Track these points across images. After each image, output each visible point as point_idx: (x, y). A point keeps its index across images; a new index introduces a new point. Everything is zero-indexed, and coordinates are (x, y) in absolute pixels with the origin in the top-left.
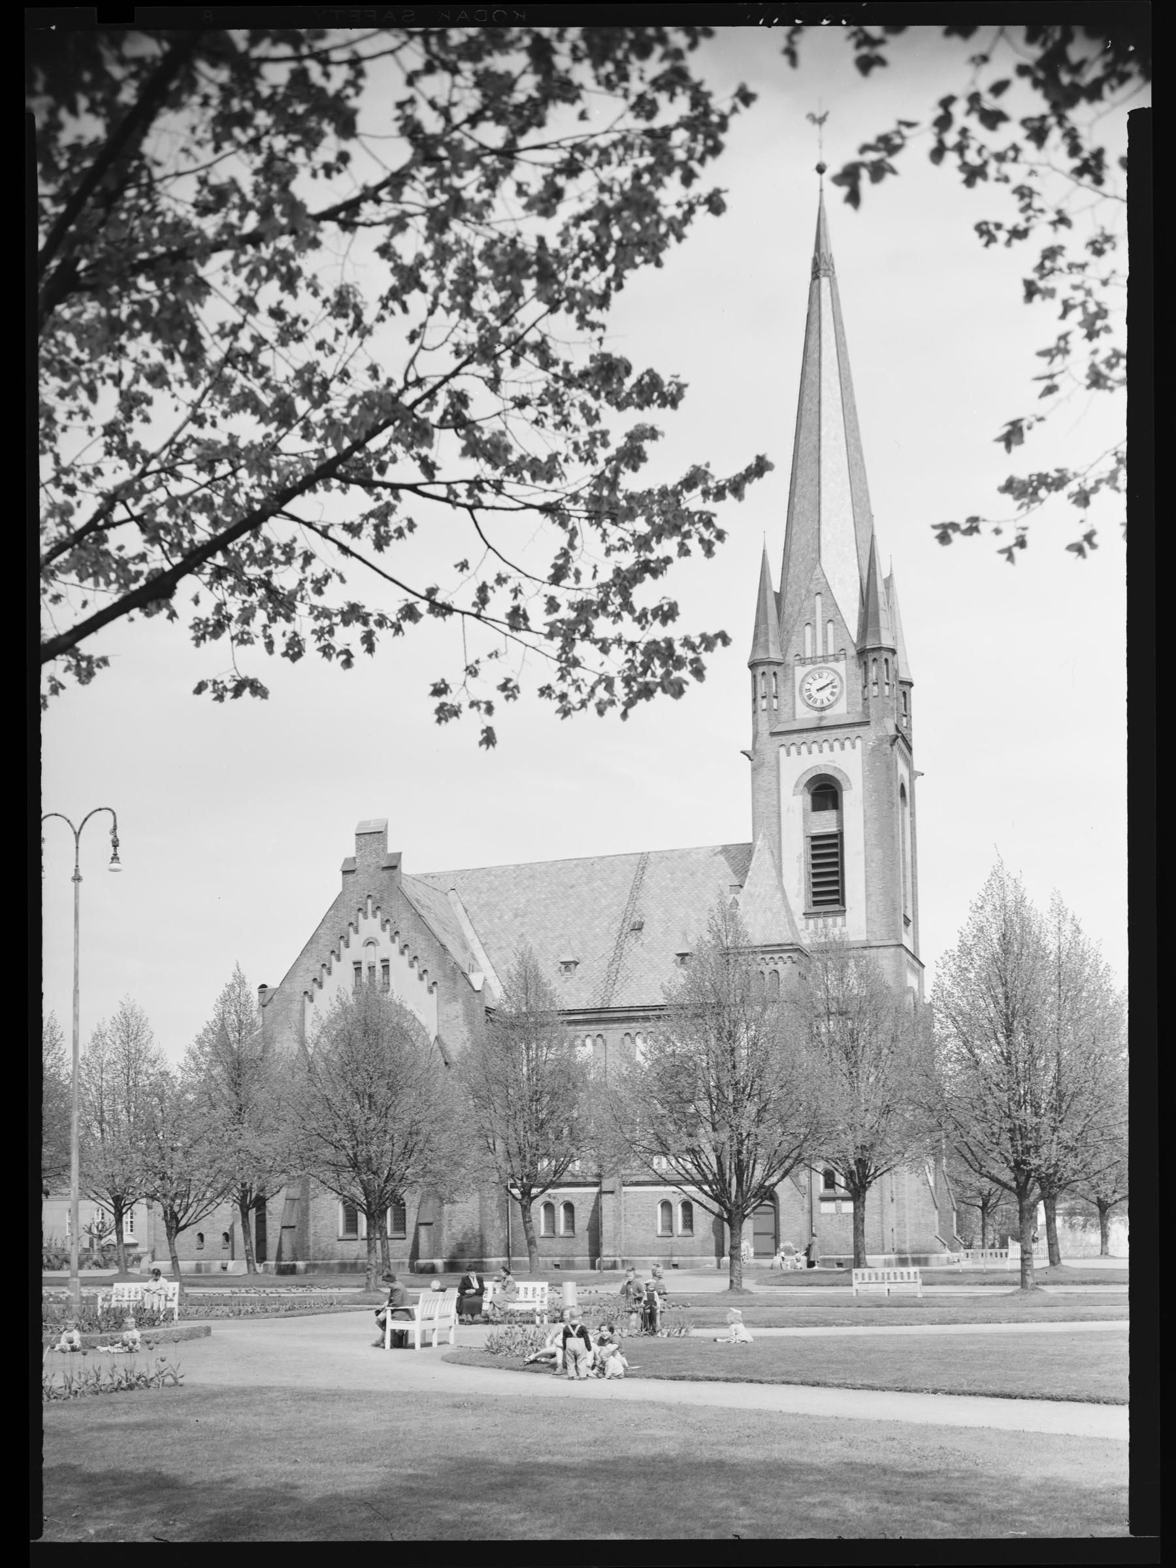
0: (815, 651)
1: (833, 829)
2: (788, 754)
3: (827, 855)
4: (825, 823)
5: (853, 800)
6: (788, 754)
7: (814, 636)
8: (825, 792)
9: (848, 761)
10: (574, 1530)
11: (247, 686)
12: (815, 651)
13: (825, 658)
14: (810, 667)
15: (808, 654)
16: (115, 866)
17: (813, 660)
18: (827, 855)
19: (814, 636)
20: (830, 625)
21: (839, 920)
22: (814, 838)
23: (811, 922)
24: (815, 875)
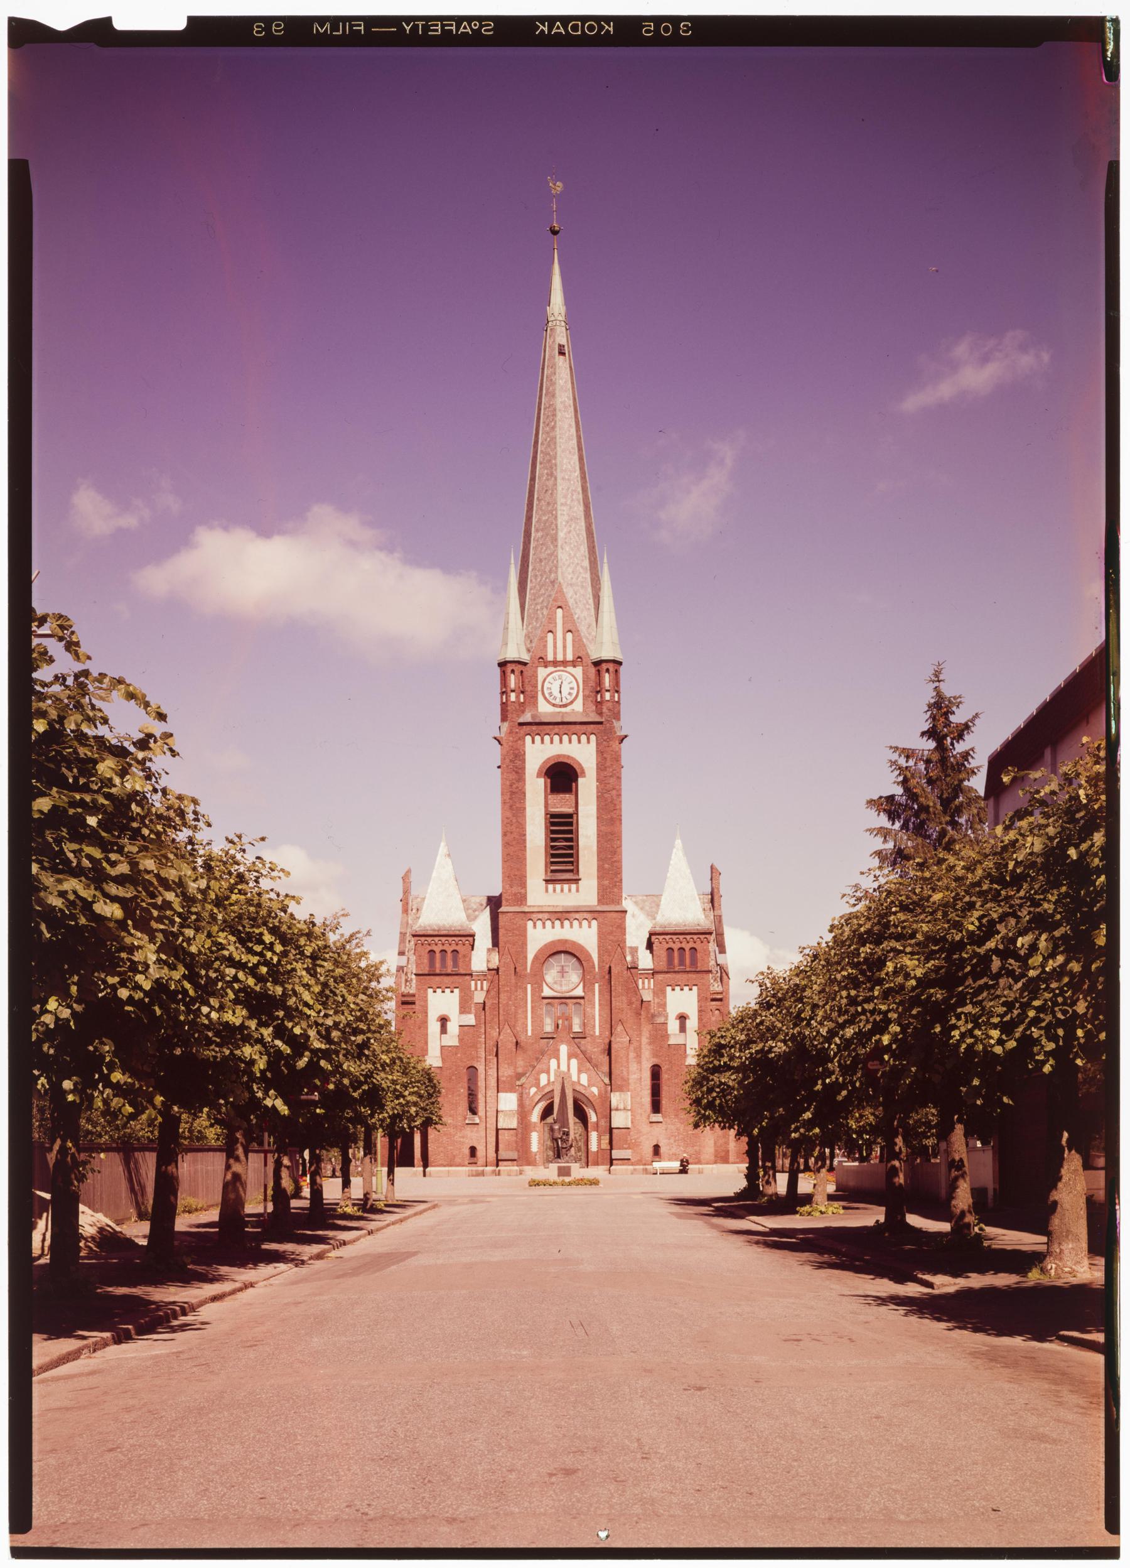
0: (555, 654)
1: (570, 810)
2: (535, 926)
3: (562, 827)
4: (562, 804)
5: (587, 787)
6: (535, 926)
7: (555, 639)
8: (561, 777)
9: (582, 752)
10: (284, 1542)
11: (594, 1182)
12: (555, 654)
13: (564, 663)
14: (550, 669)
15: (550, 658)
16: (473, 1160)
17: (555, 663)
18: (562, 827)
19: (555, 639)
20: (569, 635)
21: (574, 886)
22: (553, 816)
23: (551, 887)
24: (550, 876)
